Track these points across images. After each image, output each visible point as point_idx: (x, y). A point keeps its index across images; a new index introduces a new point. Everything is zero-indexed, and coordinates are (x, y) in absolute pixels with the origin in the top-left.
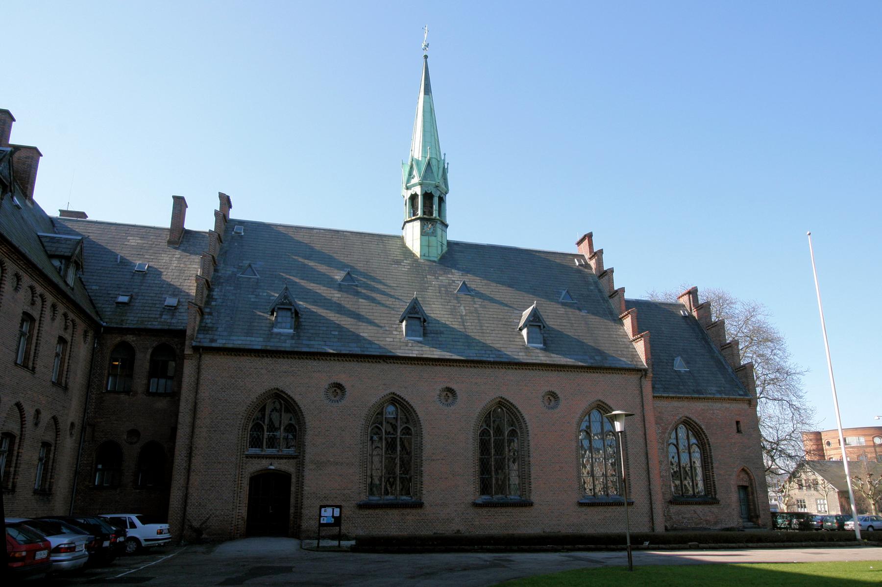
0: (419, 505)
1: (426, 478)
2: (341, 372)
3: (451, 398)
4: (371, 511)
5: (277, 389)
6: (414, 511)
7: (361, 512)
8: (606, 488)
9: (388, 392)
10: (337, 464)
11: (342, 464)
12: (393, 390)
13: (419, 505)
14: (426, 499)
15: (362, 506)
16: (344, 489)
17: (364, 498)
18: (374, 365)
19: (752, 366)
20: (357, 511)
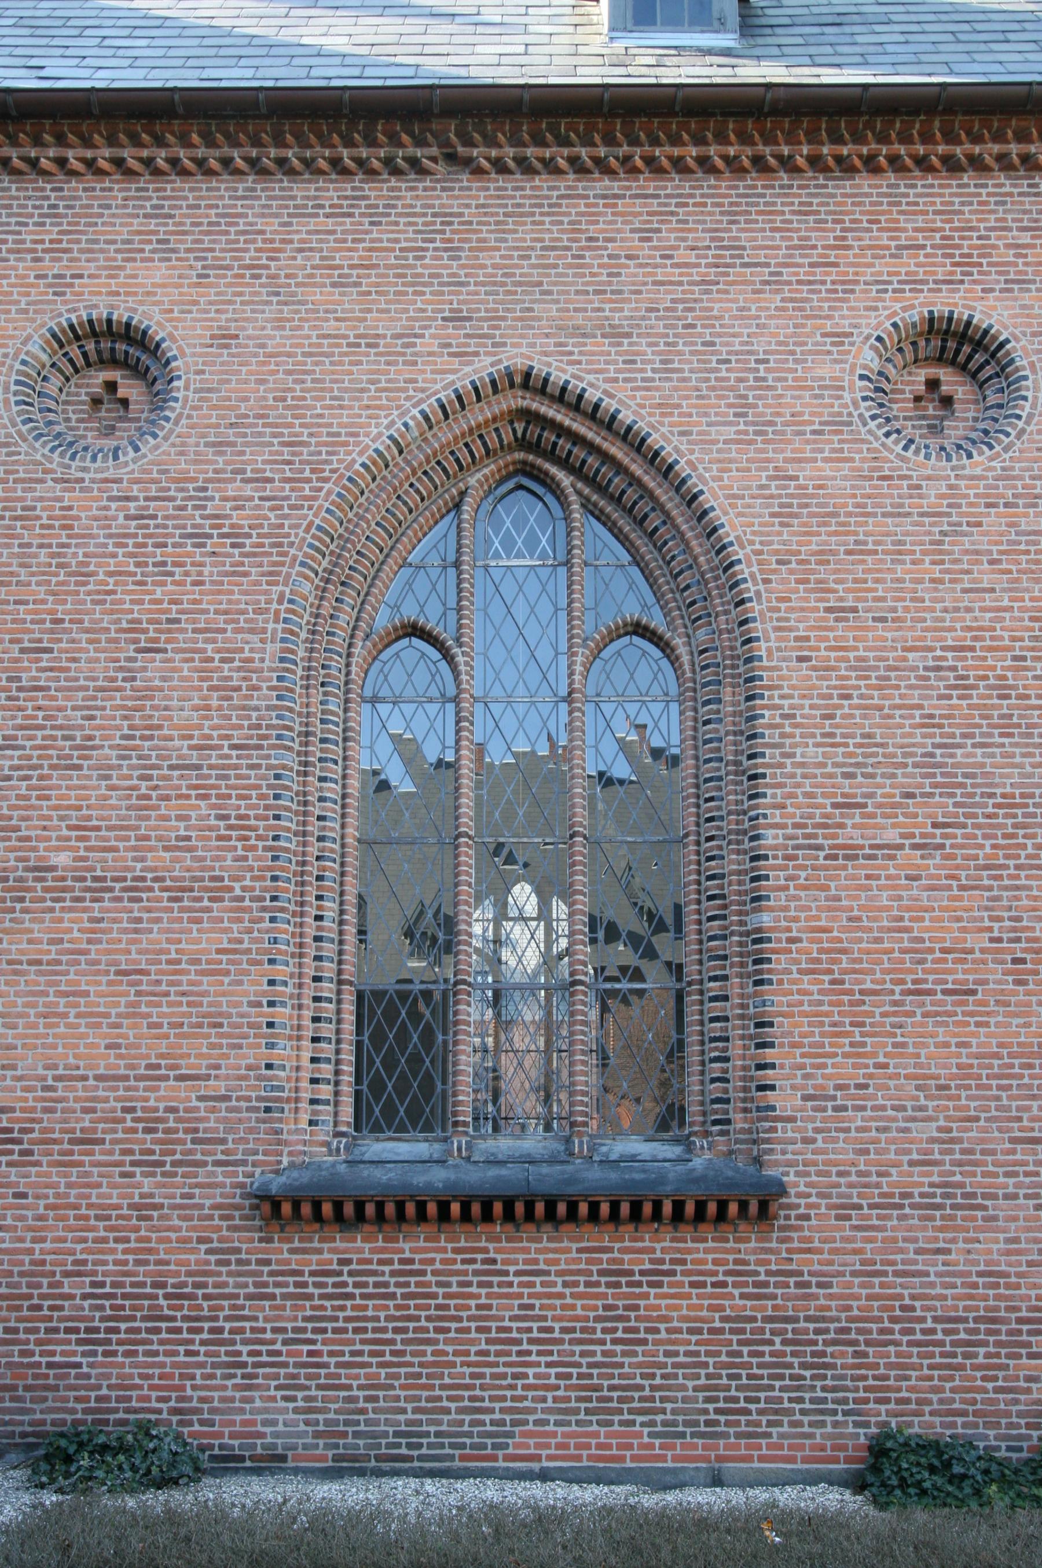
0: (748, 1204)
1: (794, 995)
2: (134, 249)
3: (966, 412)
4: (362, 1247)
5: (527, 381)
6: (705, 1250)
7: (283, 1251)
8: (777, 1163)
9: (483, 367)
10: (99, 888)
11: (136, 888)
12: (517, 356)
13: (748, 1204)
14: (800, 1156)
15: (289, 1209)
16: (153, 1075)
17: (313, 1139)
18: (376, 192)
19: (612, 29)
20: (248, 1243)
